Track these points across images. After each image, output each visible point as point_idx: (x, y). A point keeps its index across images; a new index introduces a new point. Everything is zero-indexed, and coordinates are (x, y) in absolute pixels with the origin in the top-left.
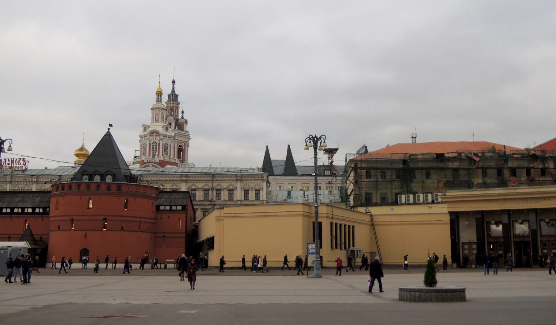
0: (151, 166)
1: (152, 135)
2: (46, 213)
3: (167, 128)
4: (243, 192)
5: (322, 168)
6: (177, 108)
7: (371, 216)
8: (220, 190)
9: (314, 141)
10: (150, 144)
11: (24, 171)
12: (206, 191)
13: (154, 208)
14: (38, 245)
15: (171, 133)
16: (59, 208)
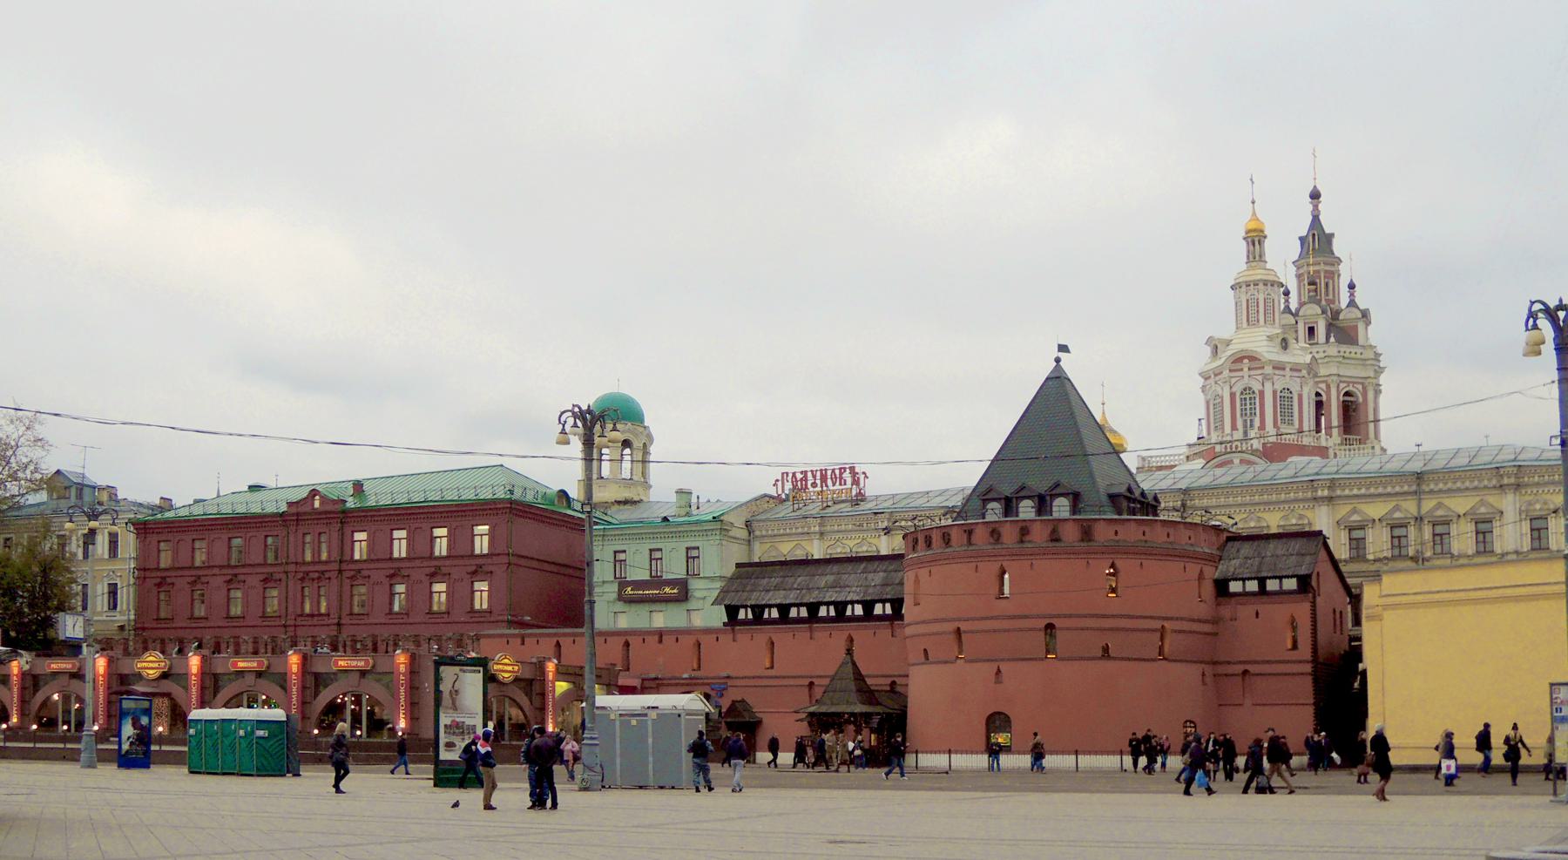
0: (1237, 461)
1: (1238, 366)
2: (897, 615)
3: (1284, 340)
4: (1526, 527)
6: (1332, 275)
8: (1447, 523)
9: (584, 420)
10: (1233, 395)
12: (1396, 527)
13: (1209, 589)
14: (879, 704)
15: (1300, 354)
16: (931, 595)
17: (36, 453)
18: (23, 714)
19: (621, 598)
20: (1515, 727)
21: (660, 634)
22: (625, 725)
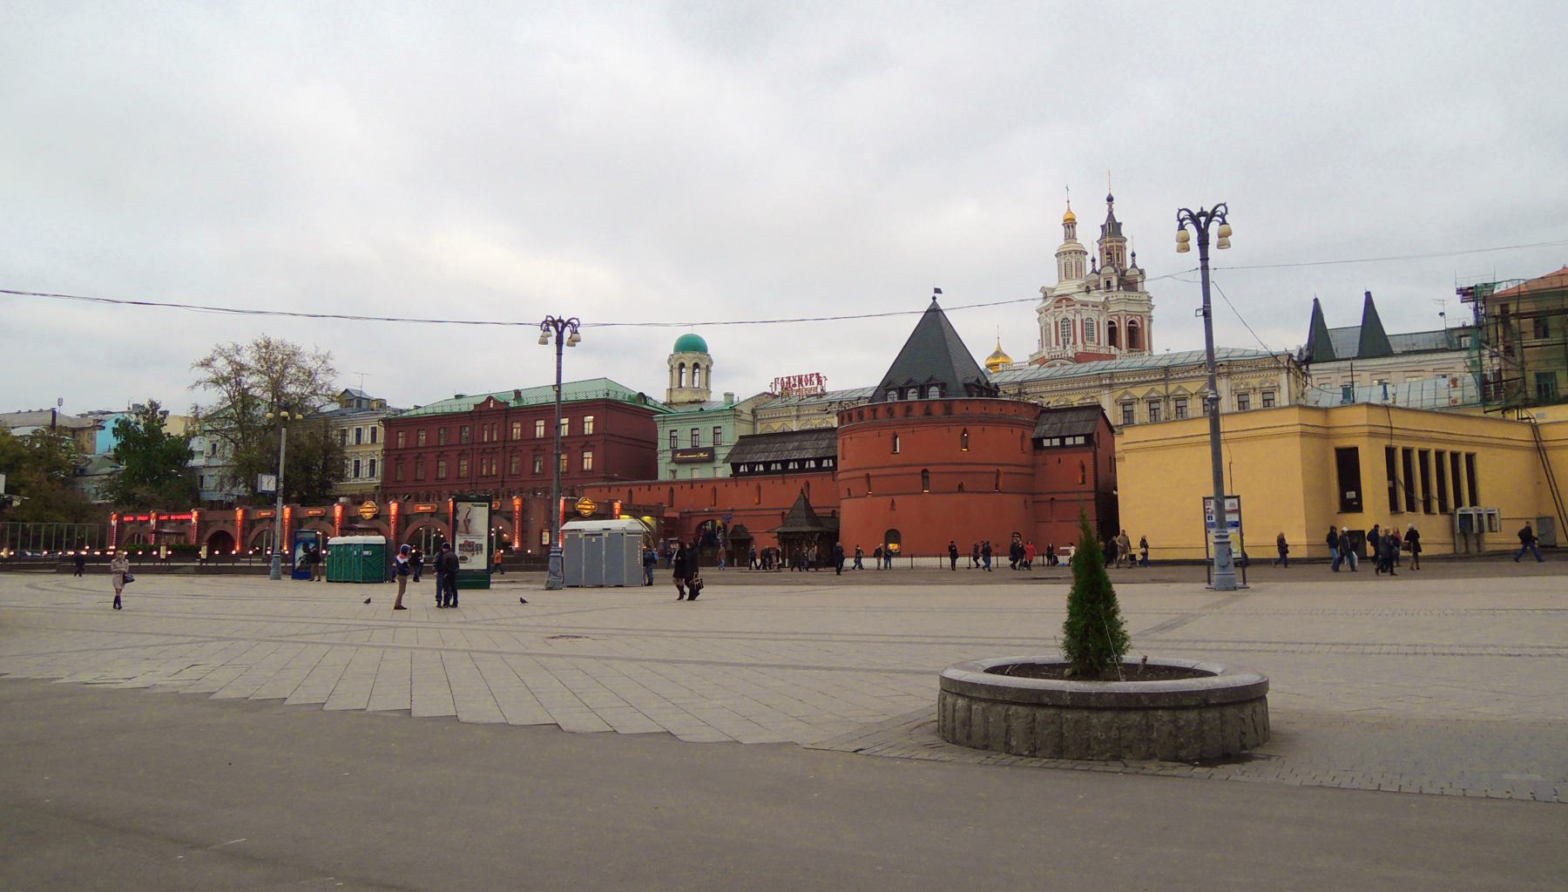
4: (1235, 399)
5: (1456, 334)
6: (1122, 249)
7: (1535, 428)
11: (820, 396)
13: (1028, 444)
16: (852, 454)
17: (329, 378)
18: (243, 545)
19: (674, 460)
20: (60, 402)
21: (692, 482)
22: (588, 543)
